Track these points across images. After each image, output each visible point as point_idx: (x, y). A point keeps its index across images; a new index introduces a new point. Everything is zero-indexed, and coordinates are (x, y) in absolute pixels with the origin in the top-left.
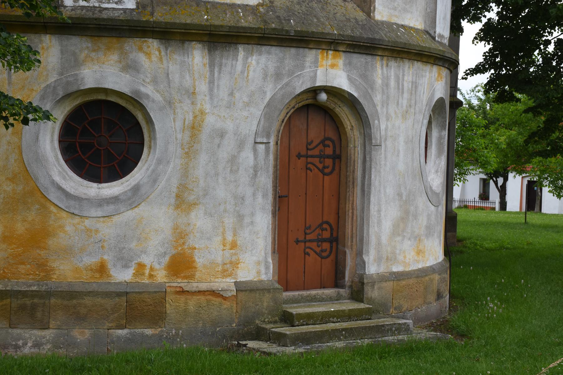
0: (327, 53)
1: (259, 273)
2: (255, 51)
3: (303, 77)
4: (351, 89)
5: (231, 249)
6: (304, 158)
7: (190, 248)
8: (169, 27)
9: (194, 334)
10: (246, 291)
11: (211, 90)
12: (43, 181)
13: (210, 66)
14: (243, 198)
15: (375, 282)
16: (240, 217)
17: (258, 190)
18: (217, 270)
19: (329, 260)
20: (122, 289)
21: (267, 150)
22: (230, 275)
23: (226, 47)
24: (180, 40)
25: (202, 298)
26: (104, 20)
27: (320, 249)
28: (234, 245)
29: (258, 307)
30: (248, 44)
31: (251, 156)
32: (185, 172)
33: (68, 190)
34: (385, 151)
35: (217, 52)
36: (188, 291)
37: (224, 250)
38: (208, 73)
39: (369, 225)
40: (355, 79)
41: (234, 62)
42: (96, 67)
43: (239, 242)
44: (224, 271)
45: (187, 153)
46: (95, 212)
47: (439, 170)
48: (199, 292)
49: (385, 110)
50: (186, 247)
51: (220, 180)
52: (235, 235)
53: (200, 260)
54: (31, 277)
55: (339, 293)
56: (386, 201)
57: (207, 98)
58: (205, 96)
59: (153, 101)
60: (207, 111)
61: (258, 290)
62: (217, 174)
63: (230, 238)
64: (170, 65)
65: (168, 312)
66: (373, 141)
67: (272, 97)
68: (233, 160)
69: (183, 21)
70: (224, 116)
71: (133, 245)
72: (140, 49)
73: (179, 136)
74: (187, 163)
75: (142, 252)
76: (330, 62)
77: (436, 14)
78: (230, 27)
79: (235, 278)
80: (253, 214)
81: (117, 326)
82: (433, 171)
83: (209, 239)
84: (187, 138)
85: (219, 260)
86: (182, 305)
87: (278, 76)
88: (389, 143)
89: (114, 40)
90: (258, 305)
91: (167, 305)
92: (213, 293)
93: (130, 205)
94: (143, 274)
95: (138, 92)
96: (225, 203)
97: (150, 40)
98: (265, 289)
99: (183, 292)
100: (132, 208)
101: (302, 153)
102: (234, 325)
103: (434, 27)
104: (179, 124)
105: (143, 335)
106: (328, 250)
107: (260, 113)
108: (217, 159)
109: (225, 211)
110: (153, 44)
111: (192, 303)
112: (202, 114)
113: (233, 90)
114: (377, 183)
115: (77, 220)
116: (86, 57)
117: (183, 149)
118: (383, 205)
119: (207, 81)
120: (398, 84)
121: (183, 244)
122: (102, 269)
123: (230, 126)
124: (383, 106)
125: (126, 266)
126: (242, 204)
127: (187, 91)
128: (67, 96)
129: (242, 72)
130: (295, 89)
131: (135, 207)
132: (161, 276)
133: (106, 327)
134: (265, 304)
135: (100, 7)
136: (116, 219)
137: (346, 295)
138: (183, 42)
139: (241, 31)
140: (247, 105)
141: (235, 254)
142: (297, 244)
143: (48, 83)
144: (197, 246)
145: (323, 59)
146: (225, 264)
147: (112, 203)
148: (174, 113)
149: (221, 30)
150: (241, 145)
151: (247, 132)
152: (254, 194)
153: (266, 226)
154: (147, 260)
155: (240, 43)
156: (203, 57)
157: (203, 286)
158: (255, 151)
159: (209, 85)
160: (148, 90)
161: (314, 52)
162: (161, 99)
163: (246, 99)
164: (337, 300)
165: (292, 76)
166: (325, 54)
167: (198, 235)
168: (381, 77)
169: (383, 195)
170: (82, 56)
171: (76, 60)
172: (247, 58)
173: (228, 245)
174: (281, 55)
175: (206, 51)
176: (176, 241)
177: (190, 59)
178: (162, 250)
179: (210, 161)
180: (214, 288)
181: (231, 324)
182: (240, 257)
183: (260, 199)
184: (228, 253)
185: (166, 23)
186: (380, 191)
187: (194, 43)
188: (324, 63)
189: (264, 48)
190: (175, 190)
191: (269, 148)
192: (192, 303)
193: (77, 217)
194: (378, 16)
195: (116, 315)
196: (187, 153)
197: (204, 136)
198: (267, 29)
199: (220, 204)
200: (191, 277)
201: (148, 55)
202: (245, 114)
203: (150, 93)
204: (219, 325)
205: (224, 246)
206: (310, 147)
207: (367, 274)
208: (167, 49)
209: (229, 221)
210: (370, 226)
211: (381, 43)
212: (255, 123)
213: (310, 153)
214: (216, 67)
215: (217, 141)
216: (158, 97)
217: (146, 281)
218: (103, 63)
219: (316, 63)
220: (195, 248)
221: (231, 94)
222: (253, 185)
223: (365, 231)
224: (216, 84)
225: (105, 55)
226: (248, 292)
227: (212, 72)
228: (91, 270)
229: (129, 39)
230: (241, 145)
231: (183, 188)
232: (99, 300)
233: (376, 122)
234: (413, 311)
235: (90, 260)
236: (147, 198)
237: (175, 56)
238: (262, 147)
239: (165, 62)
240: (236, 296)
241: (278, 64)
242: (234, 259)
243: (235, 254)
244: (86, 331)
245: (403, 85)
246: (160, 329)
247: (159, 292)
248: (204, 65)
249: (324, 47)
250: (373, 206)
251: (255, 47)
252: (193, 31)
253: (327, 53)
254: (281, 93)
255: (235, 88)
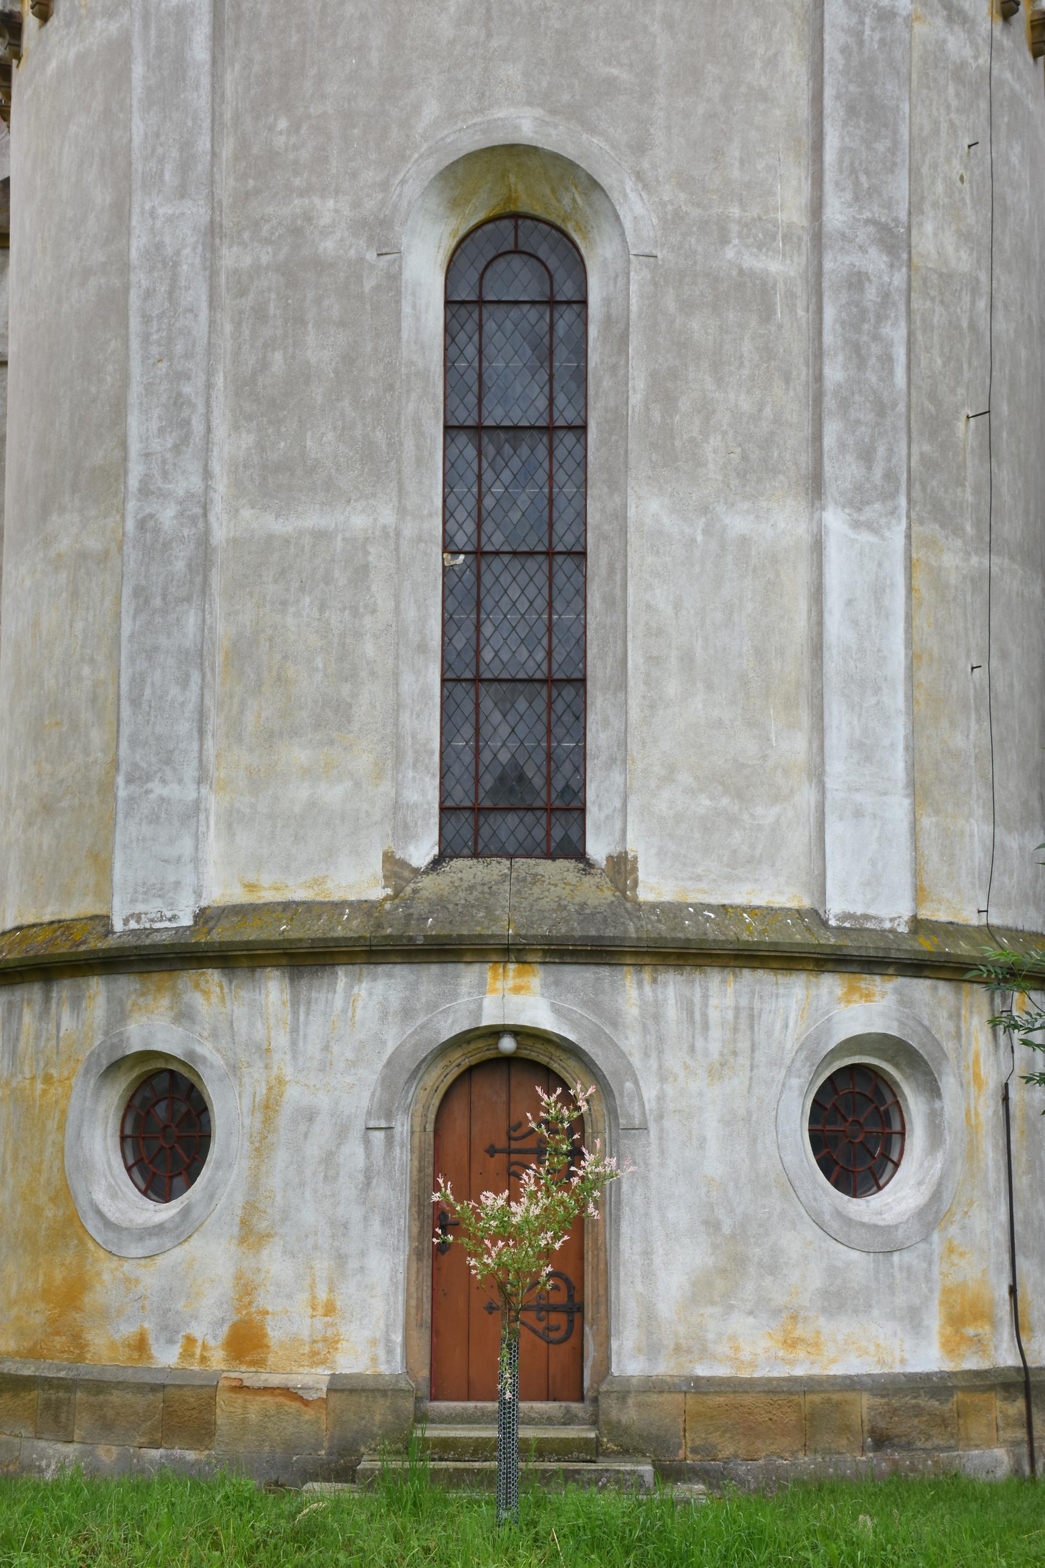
0: (504, 968)
1: (374, 1360)
2: (365, 974)
3: (455, 1012)
4: (560, 1029)
5: (325, 1315)
6: (501, 1155)
7: (259, 1313)
8: (224, 948)
9: (256, 1465)
10: (342, 1391)
11: (294, 1043)
12: (83, 1202)
13: (293, 1005)
14: (345, 1226)
15: (629, 1392)
16: (341, 1259)
17: (373, 1211)
18: (301, 1351)
19: (566, 1346)
20: (160, 1380)
21: (389, 1142)
22: (323, 1362)
23: (317, 972)
24: (248, 967)
25: (269, 1400)
26: (146, 947)
27: (544, 1324)
28: (330, 1309)
29: (363, 1422)
30: (352, 964)
31: (360, 1151)
32: (255, 1182)
33: (109, 1215)
34: (661, 1138)
35: (304, 982)
36: (248, 1387)
37: (313, 1316)
38: (289, 1017)
39: (618, 1279)
40: (569, 1010)
41: (330, 996)
42: (144, 1019)
43: (338, 1304)
44: (314, 1354)
45: (257, 1149)
46: (135, 1250)
47: (927, 1180)
48: (265, 1388)
49: (653, 1062)
50: (253, 1310)
51: (308, 1195)
52: (331, 1290)
53: (275, 1334)
54: (66, 1356)
55: (568, 1411)
56: (667, 1235)
57: (288, 1057)
58: (285, 1053)
59: (212, 1066)
60: (287, 1079)
61: (363, 1390)
62: (302, 1184)
63: (323, 1295)
64: (235, 1008)
65: (219, 1422)
66: (622, 1121)
67: (396, 1049)
68: (329, 1159)
69: (245, 938)
70: (315, 1086)
71: (180, 1305)
72: (197, 986)
73: (247, 1121)
74: (257, 1167)
75: (192, 1316)
76: (510, 983)
77: (825, 878)
78: (313, 940)
79: (332, 1368)
80: (363, 1254)
81: (150, 1443)
82: (912, 1182)
83: (289, 1296)
84: (258, 1125)
85: (305, 1334)
86: (240, 1411)
87: (407, 1013)
88: (671, 1124)
89: (166, 975)
90: (363, 1418)
91: (218, 1410)
92: (287, 1392)
93: (178, 1237)
94: (192, 1355)
95: (191, 1054)
96: (316, 1234)
97: (210, 971)
98: (378, 1390)
99: (240, 1388)
100: (181, 1243)
101: (498, 1146)
102: (323, 1452)
103: (823, 902)
104: (246, 1102)
105: (182, 1460)
106: (564, 1327)
107: (375, 1077)
108: (304, 1158)
109: (316, 1247)
110: (213, 976)
111: (255, 1408)
112: (280, 1082)
113: (328, 1042)
114: (638, 1200)
115: (115, 1263)
116: (133, 1005)
117: (252, 1143)
118: (659, 1243)
119: (288, 1029)
120: (691, 1013)
121: (250, 1303)
122: (141, 1345)
123: (323, 1101)
124: (647, 1055)
125: (171, 1341)
126: (344, 1235)
127: (258, 1048)
128: (115, 1067)
129: (344, 1011)
130: (438, 1033)
131: (185, 1241)
132: (218, 1361)
133: (135, 1444)
134: (378, 1418)
135: (151, 929)
136: (160, 1261)
137: (587, 1416)
138: (253, 969)
139: (331, 945)
140: (353, 1064)
141: (333, 1325)
142: (490, 1313)
143: (93, 1048)
144: (270, 1309)
145: (495, 978)
146: (315, 1342)
147: (156, 1235)
148: (241, 1086)
149: (299, 945)
150: (342, 1133)
151: (353, 1111)
152: (366, 1219)
153: (388, 1275)
154: (199, 1330)
155: (339, 964)
156: (282, 991)
157: (275, 1380)
158: (367, 1143)
159: (291, 1036)
160: (205, 1049)
161: (476, 968)
162: (222, 1062)
163: (350, 1055)
164: (565, 1424)
165: (433, 1011)
166: (501, 970)
167: (272, 1289)
168: (638, 1003)
169: (656, 1223)
170: (129, 1004)
171: (122, 1012)
172: (352, 987)
173: (320, 1307)
174: (412, 978)
175: (287, 980)
176: (239, 1300)
177: (263, 996)
178: (219, 1314)
179: (292, 1162)
180: (290, 1384)
181: (316, 1451)
182: (342, 1330)
183: (376, 1227)
184: (320, 1322)
185: (221, 943)
186: (646, 1214)
187: (269, 969)
188: (499, 985)
189: (380, 969)
190: (239, 1212)
191: (393, 1137)
192: (255, 1408)
193: (115, 1258)
194: (644, 895)
195: (149, 1423)
196: (257, 1149)
197: (283, 1120)
198: (375, 937)
199: (307, 1236)
200: (259, 1363)
201: (206, 994)
202: (349, 1079)
203: (207, 1054)
204: (297, 1450)
205: (314, 1309)
206: (514, 1134)
207: (615, 1374)
208: (230, 982)
209: (322, 1266)
210: (621, 1281)
211: (618, 943)
212: (367, 1094)
213: (515, 1145)
214: (302, 1006)
215: (303, 1127)
216: (217, 1060)
217: (196, 1368)
218: (152, 1013)
219: (481, 987)
220: (267, 1313)
221: (326, 1048)
222: (364, 1203)
223: (613, 1292)
224: (301, 1033)
225: (154, 1000)
226: (346, 1393)
227: (295, 1013)
228: (129, 1346)
229: (183, 973)
230: (342, 1133)
231: (251, 1208)
232: (129, 1396)
233: (629, 1085)
234: (761, 1462)
235: (127, 1330)
236: (201, 1226)
237: (243, 993)
238: (380, 1135)
239: (228, 1003)
240: (325, 1401)
241: (408, 993)
242: (329, 1333)
243: (333, 1325)
244: (113, 1448)
245: (704, 1015)
246: (207, 1452)
247: (206, 1386)
248: (284, 1003)
249: (495, 959)
250: (628, 1244)
251: (365, 968)
252: (260, 952)
253: (504, 968)
254: (413, 1042)
255: (333, 1038)
